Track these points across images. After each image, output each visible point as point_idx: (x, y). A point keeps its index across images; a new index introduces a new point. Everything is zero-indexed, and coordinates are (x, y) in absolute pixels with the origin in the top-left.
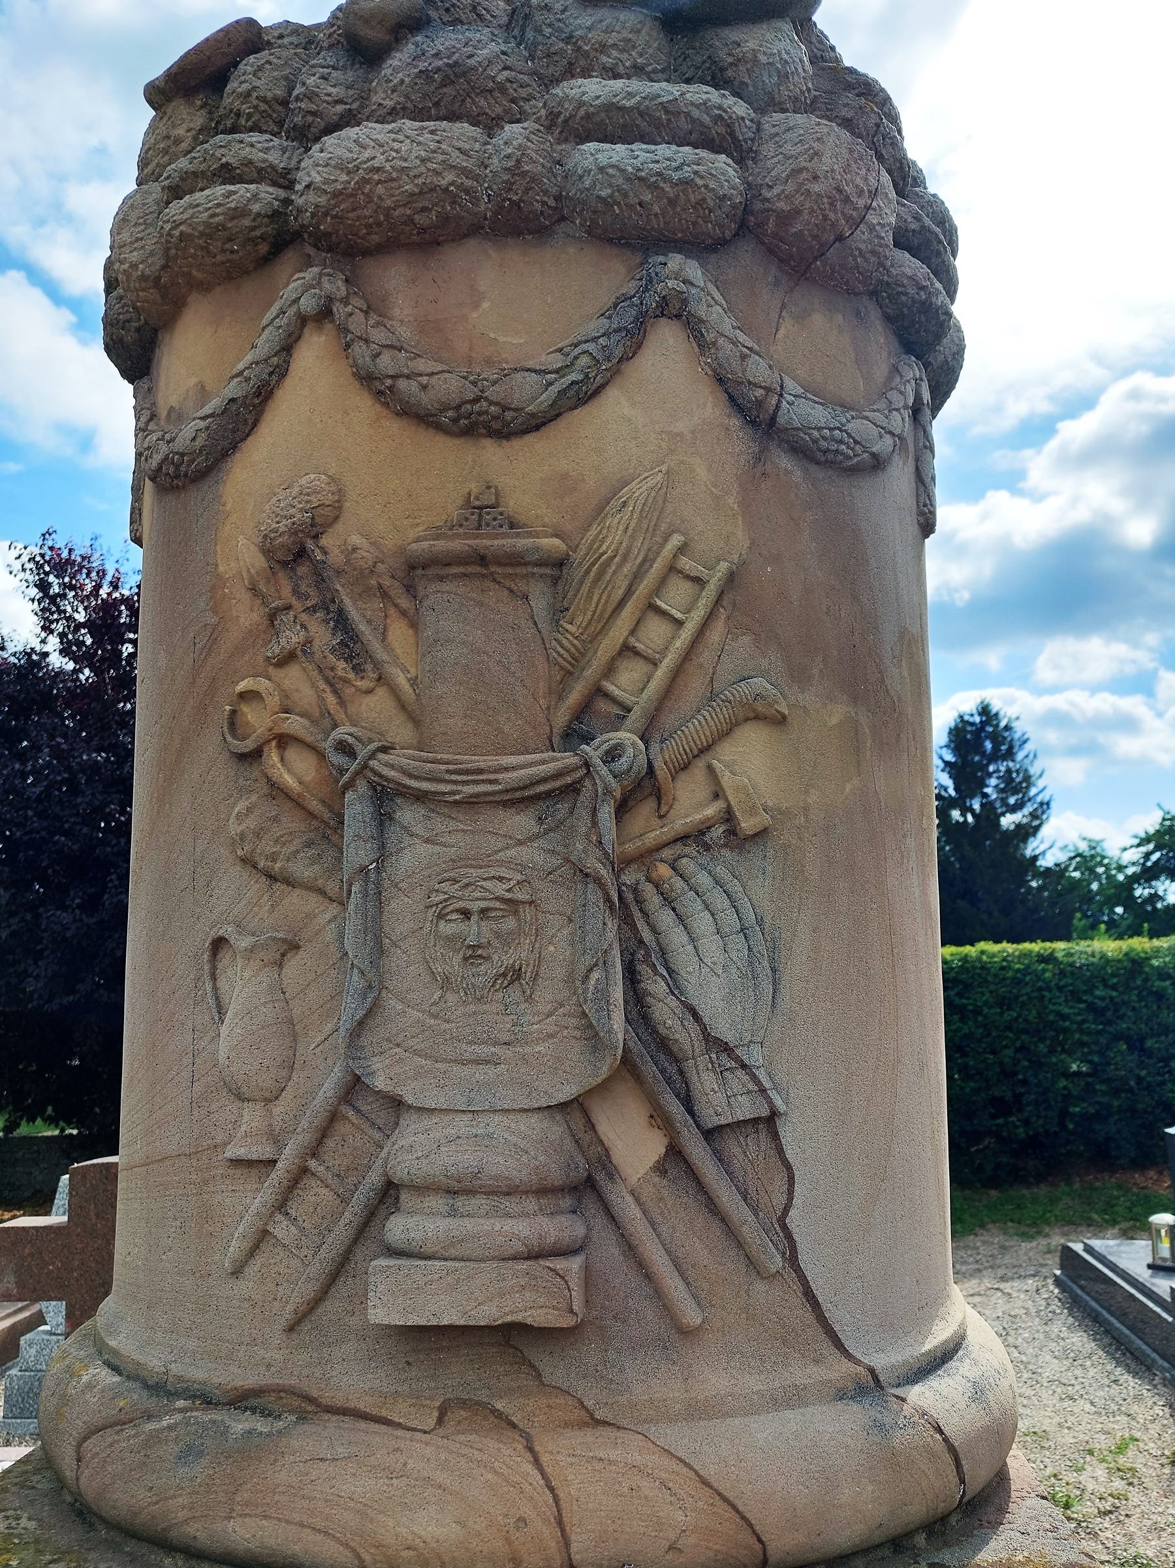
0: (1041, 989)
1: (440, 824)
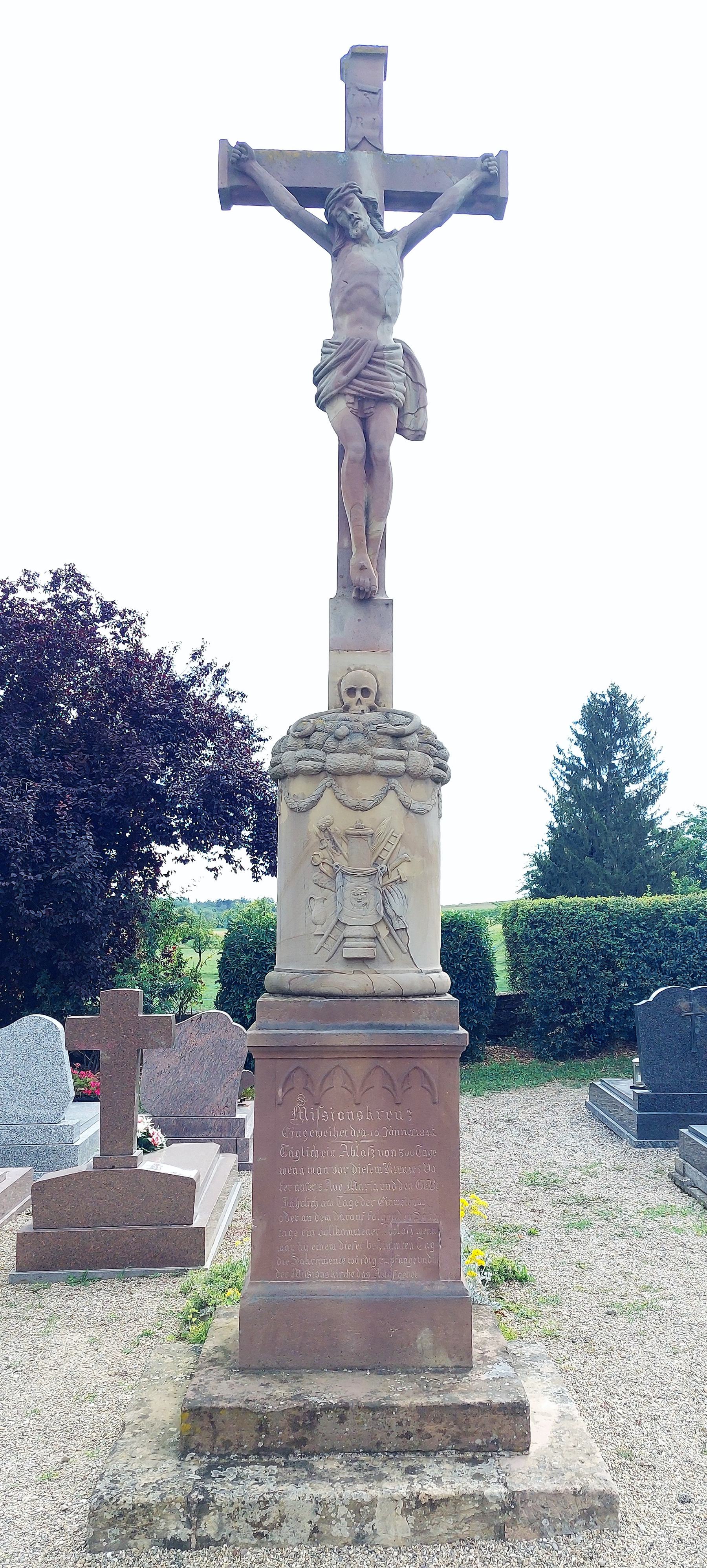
0: (596, 928)
1: (353, 879)
